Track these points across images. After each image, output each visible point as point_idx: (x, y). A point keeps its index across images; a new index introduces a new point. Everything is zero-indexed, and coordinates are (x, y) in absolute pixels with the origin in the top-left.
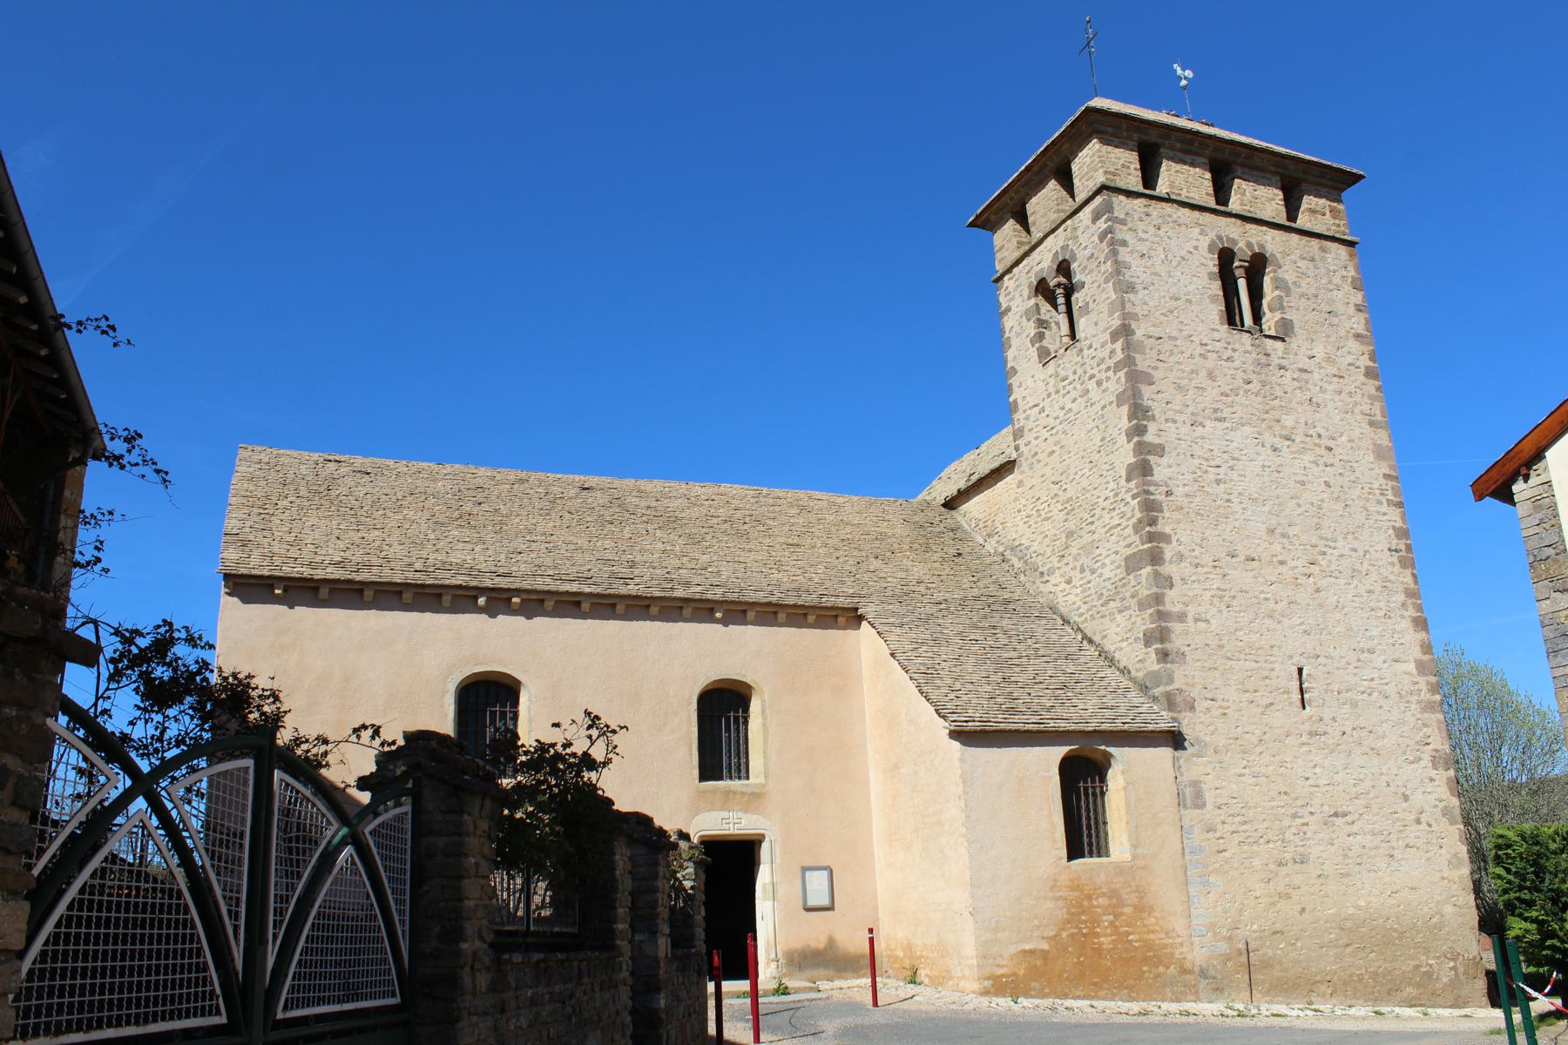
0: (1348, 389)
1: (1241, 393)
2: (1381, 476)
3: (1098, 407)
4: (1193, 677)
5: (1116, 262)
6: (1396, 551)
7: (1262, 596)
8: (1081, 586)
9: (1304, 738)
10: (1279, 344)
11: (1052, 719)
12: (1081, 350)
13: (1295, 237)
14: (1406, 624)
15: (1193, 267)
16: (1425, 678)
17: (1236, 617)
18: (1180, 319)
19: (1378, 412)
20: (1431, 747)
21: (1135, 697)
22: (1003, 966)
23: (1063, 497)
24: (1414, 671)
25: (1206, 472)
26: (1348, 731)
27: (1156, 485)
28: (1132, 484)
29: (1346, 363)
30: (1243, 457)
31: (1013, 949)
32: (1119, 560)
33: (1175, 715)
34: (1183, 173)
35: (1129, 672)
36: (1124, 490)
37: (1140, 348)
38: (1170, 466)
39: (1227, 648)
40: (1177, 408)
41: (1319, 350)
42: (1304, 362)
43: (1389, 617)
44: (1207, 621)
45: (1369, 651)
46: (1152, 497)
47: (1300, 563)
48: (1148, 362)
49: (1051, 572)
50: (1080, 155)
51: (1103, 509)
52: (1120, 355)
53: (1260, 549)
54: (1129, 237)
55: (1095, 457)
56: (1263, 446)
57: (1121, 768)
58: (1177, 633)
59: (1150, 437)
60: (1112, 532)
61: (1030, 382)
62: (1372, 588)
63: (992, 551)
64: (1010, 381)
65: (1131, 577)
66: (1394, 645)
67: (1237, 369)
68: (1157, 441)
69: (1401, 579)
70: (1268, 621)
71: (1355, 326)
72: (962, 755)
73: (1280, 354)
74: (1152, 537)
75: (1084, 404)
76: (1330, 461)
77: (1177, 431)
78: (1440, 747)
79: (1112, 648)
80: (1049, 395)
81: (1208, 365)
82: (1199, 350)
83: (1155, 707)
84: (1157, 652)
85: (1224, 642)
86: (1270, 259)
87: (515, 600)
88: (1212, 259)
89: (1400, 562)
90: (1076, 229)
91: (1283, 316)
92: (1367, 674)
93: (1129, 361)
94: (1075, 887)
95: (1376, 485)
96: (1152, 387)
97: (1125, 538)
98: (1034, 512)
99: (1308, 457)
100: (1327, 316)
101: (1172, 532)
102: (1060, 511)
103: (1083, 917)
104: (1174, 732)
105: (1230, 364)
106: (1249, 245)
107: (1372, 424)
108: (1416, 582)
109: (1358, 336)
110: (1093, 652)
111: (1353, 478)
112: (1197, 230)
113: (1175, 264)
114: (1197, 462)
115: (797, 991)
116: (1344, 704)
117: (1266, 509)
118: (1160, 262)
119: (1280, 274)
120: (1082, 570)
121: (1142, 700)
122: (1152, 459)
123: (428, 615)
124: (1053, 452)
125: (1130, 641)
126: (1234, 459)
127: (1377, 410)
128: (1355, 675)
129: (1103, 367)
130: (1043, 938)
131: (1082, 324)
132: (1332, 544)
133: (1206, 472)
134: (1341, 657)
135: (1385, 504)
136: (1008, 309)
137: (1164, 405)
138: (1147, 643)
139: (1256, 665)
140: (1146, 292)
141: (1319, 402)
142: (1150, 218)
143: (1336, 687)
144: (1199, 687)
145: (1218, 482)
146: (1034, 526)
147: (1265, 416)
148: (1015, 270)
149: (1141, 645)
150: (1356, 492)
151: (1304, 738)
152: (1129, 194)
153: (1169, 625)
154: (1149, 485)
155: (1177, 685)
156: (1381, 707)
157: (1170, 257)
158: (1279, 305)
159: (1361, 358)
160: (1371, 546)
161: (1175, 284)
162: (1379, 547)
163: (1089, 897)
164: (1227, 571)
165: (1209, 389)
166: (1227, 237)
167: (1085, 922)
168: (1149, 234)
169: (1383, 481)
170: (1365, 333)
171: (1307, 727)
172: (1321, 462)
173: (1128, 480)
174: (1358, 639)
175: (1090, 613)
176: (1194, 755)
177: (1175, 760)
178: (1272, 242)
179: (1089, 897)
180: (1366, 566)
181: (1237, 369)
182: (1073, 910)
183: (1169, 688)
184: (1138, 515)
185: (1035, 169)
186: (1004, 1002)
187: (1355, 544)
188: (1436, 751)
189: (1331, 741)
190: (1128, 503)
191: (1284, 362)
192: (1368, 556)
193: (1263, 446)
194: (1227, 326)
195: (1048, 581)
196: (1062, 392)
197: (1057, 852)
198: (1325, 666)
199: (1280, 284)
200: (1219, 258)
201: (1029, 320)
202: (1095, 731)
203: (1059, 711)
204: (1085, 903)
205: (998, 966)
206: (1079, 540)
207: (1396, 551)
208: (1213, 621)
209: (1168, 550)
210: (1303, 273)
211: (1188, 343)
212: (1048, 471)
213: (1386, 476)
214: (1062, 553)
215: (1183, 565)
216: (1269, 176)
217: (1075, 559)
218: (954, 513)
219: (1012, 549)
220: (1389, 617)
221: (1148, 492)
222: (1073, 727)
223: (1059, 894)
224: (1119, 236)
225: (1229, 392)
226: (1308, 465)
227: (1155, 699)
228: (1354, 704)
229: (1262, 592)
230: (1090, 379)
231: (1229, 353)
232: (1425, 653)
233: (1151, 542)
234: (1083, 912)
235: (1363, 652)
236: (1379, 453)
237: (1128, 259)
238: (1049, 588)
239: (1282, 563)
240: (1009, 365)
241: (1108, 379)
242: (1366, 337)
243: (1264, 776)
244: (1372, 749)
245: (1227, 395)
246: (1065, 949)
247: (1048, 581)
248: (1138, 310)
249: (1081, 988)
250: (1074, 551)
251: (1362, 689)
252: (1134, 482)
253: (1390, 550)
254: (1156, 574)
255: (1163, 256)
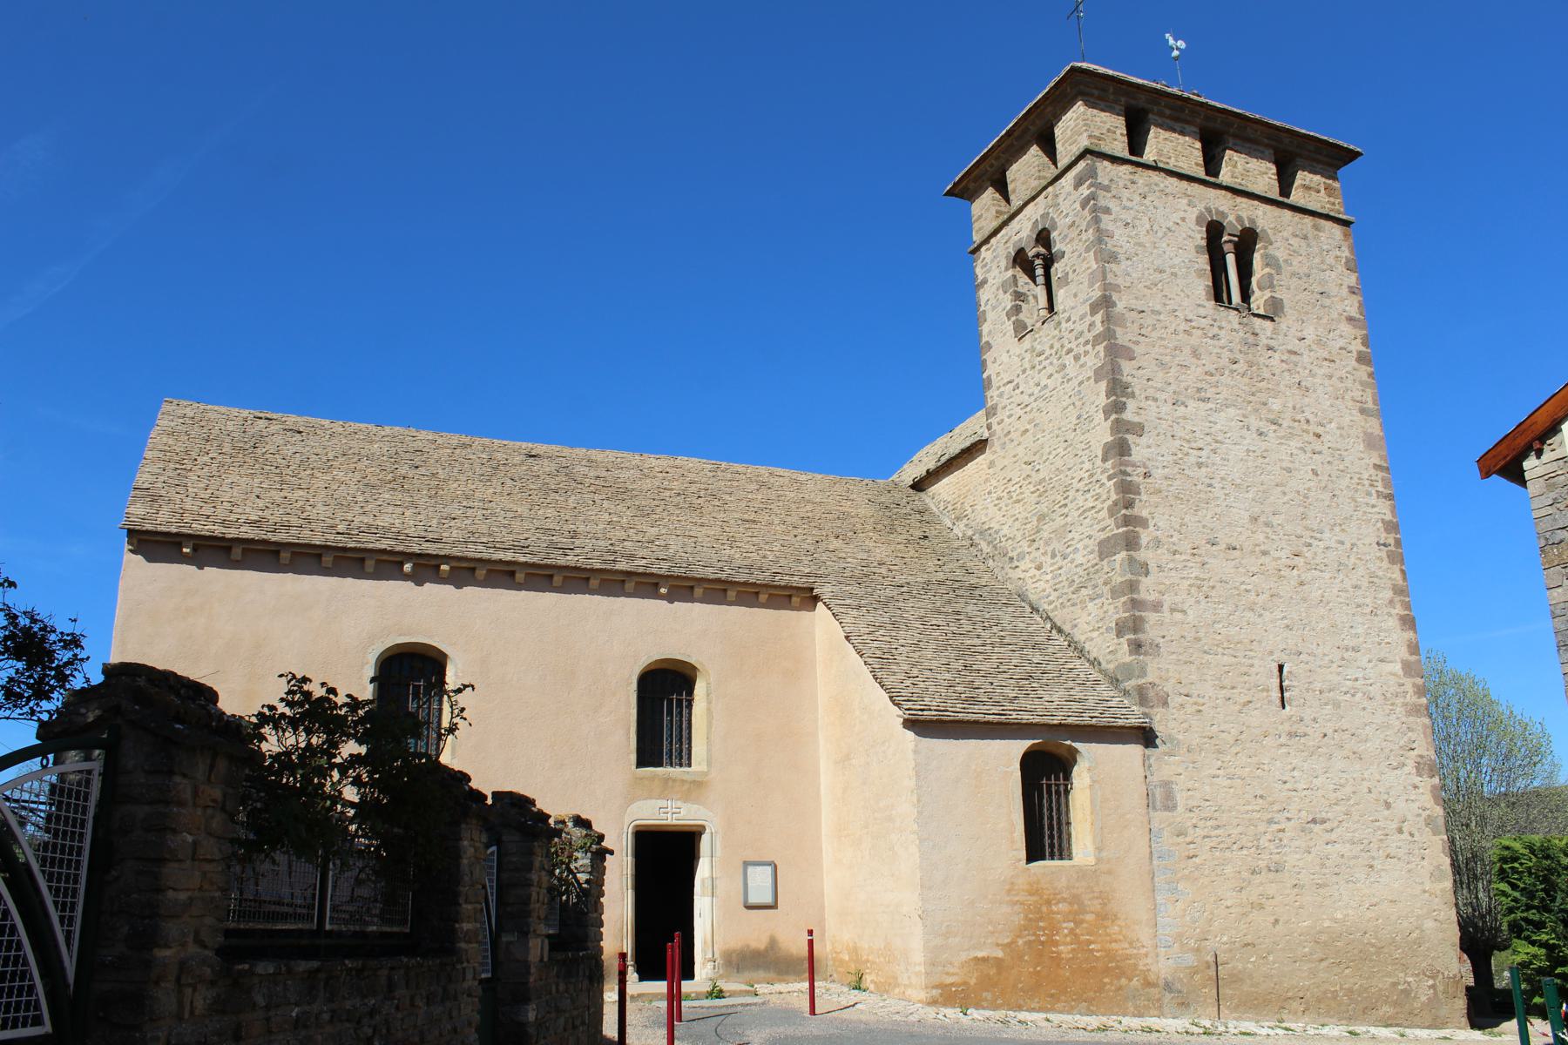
0: (1338, 374)
1: (1227, 372)
2: (1371, 466)
3: (1075, 382)
4: (1168, 670)
5: (1098, 230)
6: (1385, 545)
7: (1243, 587)
8: (1051, 572)
9: (1283, 740)
10: (1268, 323)
11: (1014, 710)
12: (1059, 323)
13: (1287, 213)
14: (1393, 623)
15: (1180, 240)
16: (1413, 680)
17: (1215, 609)
18: (1164, 293)
19: (1370, 400)
20: (1416, 752)
21: (1105, 690)
22: (953, 974)
23: (1036, 477)
24: (1401, 672)
25: (1187, 454)
26: (1330, 732)
27: (1134, 465)
28: (1109, 464)
29: (1338, 346)
30: (1227, 441)
31: (964, 956)
32: (1093, 545)
33: (1147, 710)
34: (1172, 141)
35: (1100, 664)
36: (1099, 470)
37: (1121, 321)
38: (1149, 447)
39: (1204, 641)
40: (1159, 385)
41: (1310, 332)
42: (1294, 344)
43: (1376, 615)
44: (1184, 612)
45: (1353, 649)
46: (1129, 479)
47: (1283, 554)
48: (1130, 336)
49: (1021, 557)
50: (1064, 118)
51: (1078, 491)
52: (1099, 328)
53: (1243, 538)
54: (1112, 205)
55: (1071, 435)
56: (1248, 429)
57: (1087, 765)
58: (1151, 623)
59: (1129, 415)
60: (1086, 515)
61: (1005, 357)
62: (1359, 583)
63: (960, 535)
64: (984, 357)
65: (1105, 562)
66: (1380, 644)
67: (1223, 348)
68: (1136, 419)
69: (1389, 575)
70: (1249, 614)
71: (1347, 308)
72: (916, 746)
73: (1269, 334)
74: (1127, 521)
75: (1061, 380)
76: (1318, 448)
77: (1157, 410)
78: (1425, 753)
79: (1082, 638)
80: (1024, 371)
81: (1192, 342)
82: (1183, 326)
83: (1126, 702)
84: (1130, 643)
85: (1201, 634)
86: (1261, 235)
87: (444, 567)
88: (1199, 232)
89: (1388, 557)
90: (1057, 196)
91: (1273, 294)
92: (1352, 673)
93: (1108, 335)
94: (1034, 891)
95: (1366, 476)
96: (1133, 362)
97: (1099, 522)
98: (1005, 494)
99: (1294, 444)
100: (1319, 296)
101: (1149, 516)
102: (1032, 493)
103: (1041, 924)
104: (1144, 728)
105: (1216, 342)
106: (1239, 219)
107: (1363, 411)
108: (1405, 579)
109: (1350, 319)
110: (1061, 641)
111: (1341, 467)
112: (1185, 201)
113: (1160, 234)
114: (1177, 443)
115: (733, 994)
116: (1326, 704)
117: (1250, 495)
118: (1145, 232)
119: (1271, 250)
120: (1054, 556)
121: (1112, 693)
122: (1130, 438)
123: (349, 580)
124: (1027, 431)
125: (1101, 630)
126: (1217, 442)
127: (1368, 397)
128: (1339, 674)
129: (1082, 340)
130: (998, 945)
131: (1060, 295)
132: (1319, 536)
133: (1187, 454)
134: (1325, 655)
135: (1375, 495)
136: (985, 282)
137: (1145, 382)
138: (1119, 634)
139: (1233, 659)
140: (1129, 263)
141: (1309, 385)
142: (1135, 186)
143: (1318, 686)
144: (1173, 681)
145: (1200, 465)
146: (1004, 508)
147: (1252, 398)
148: (993, 241)
149: (1113, 635)
150: (1345, 482)
151: (1283, 740)
152: (1114, 159)
153: (1143, 614)
154: (1127, 465)
155: (1149, 679)
156: (1364, 709)
157: (1155, 228)
158: (1269, 284)
159: (1354, 342)
160: (1359, 539)
161: (1160, 256)
162: (1367, 541)
163: (1049, 902)
164: (1206, 559)
165: (1193, 368)
166: (1217, 209)
167: (1044, 929)
168: (1134, 203)
169: (1373, 471)
170: (1358, 316)
171: (1286, 727)
172: (1309, 448)
173: (1104, 460)
174: (1343, 636)
175: (1060, 601)
176: (1166, 754)
177: (1145, 758)
178: (1263, 217)
179: (1049, 902)
180: (1353, 560)
181: (1223, 348)
182: (1031, 916)
183: (1141, 681)
184: (1114, 497)
185: (1016, 134)
186: (952, 1013)
187: (1342, 537)
188: (1421, 757)
189: (1311, 743)
190: (1103, 484)
191: (1272, 343)
192: (1355, 549)
193: (1248, 429)
194: (1213, 302)
195: (1017, 567)
196: (1038, 367)
197: (1015, 853)
198: (1307, 663)
199: (1270, 261)
200: (1207, 231)
201: (1005, 292)
202: (1060, 725)
203: (1023, 703)
204: (1044, 909)
205: (947, 974)
206: (1052, 523)
207: (1385, 545)
208: (1190, 612)
209: (1145, 537)
210: (1294, 251)
211: (1172, 318)
212: (1020, 450)
213: (1376, 467)
214: (1034, 537)
215: (1159, 551)
216: (1261, 148)
217: (1047, 544)
218: (922, 495)
219: (981, 533)
220: (1376, 615)
221: (1125, 473)
222: (1037, 720)
223: (1016, 899)
224: (1102, 202)
225: (1214, 372)
226: (1295, 452)
227: (1126, 693)
228: (1337, 705)
229: (1243, 583)
230: (1068, 353)
231: (1215, 330)
232: (1412, 654)
233: (1127, 526)
234: (1041, 919)
235: (1347, 650)
236: (1370, 442)
237: (1111, 227)
238: (1018, 573)
239: (1265, 553)
240: (984, 340)
241: (1086, 353)
242: (1359, 320)
243: (1238, 778)
244: (1354, 753)
245: (1212, 375)
246: (1021, 958)
247: (1017, 567)
248: (1120, 281)
249: (1036, 1000)
250: (1045, 535)
251: (1344, 689)
252: (1110, 462)
253: (1378, 544)
254: (1131, 560)
255: (1148, 226)
